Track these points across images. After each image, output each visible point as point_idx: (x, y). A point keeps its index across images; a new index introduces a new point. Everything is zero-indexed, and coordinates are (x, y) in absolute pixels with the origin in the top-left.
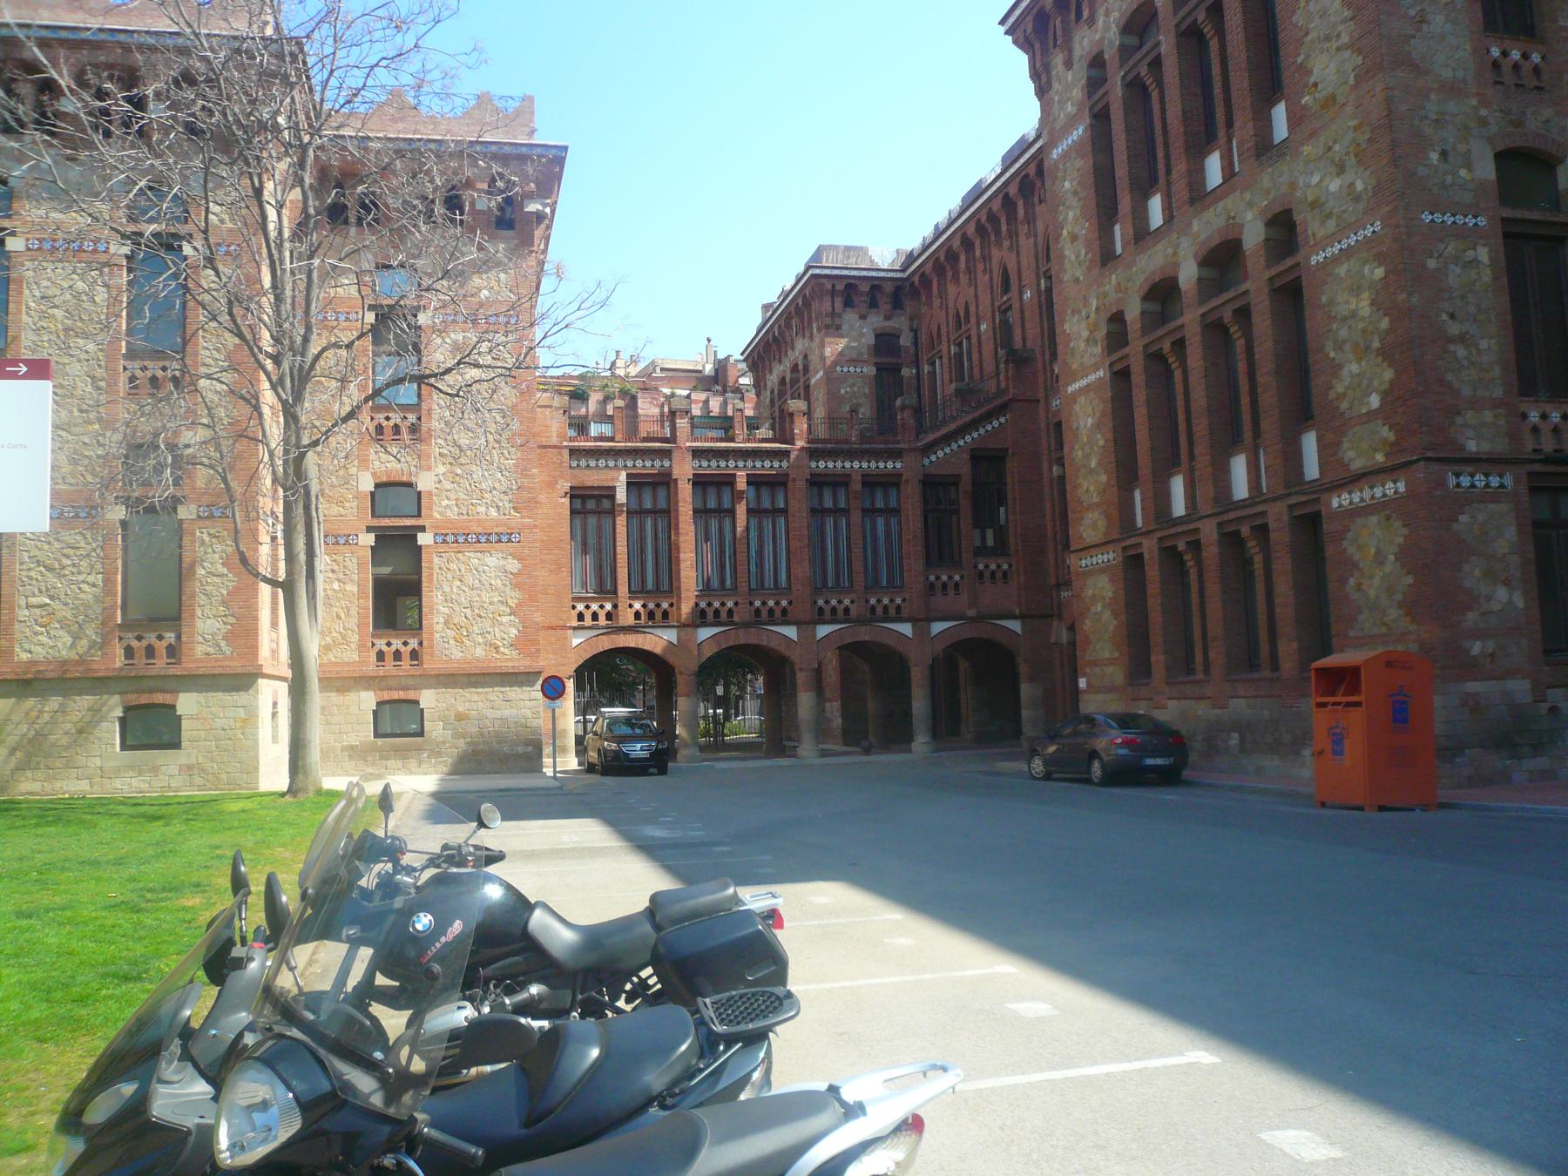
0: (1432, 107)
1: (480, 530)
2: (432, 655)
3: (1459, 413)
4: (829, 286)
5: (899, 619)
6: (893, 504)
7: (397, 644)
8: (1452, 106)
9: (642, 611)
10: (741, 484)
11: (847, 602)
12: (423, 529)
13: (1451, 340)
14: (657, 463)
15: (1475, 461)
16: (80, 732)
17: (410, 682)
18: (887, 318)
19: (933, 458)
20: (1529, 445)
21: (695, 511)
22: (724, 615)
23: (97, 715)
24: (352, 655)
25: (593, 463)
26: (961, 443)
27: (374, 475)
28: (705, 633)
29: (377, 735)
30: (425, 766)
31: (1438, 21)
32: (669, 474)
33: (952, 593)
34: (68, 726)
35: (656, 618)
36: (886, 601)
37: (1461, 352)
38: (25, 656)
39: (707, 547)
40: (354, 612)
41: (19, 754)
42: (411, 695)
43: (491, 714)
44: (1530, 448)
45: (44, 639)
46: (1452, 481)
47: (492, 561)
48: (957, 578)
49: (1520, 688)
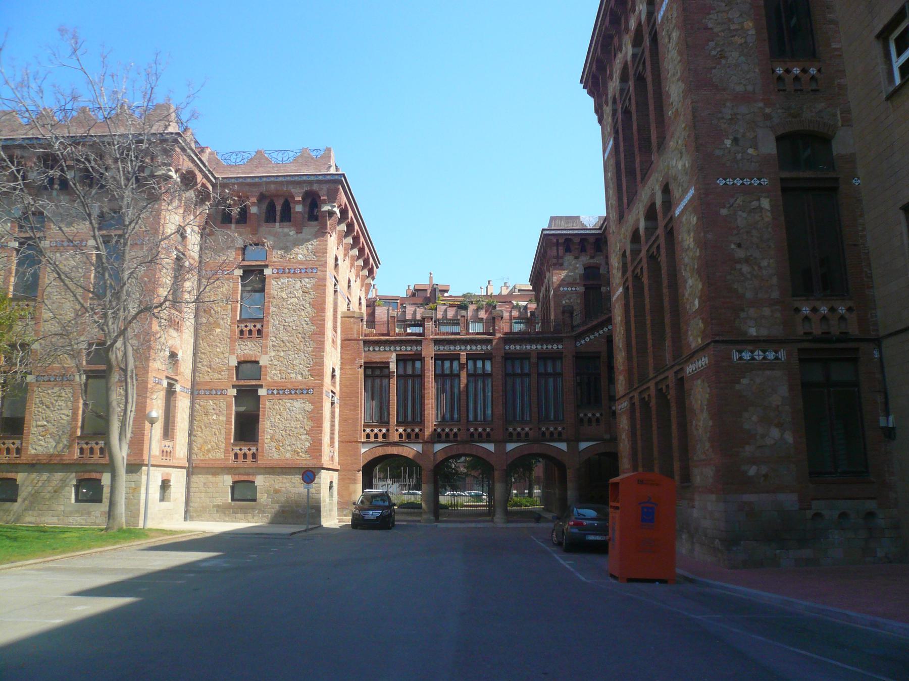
0: (727, 112)
1: (291, 387)
2: (263, 456)
3: (743, 310)
4: (555, 241)
5: (560, 440)
6: (559, 370)
7: (245, 450)
8: (743, 109)
9: (403, 433)
10: (463, 360)
11: (527, 429)
12: (261, 386)
13: (739, 261)
14: (414, 348)
15: (755, 342)
16: (55, 492)
17: (251, 471)
18: (592, 257)
19: (583, 342)
20: (800, 330)
21: (436, 375)
22: (451, 436)
23: (64, 484)
24: (220, 455)
25: (377, 349)
26: (601, 332)
27: (237, 357)
28: (438, 447)
29: (233, 499)
30: (256, 518)
31: (734, 56)
32: (421, 354)
33: (594, 424)
34: (50, 489)
35: (411, 437)
36: (552, 429)
37: (745, 269)
38: (33, 452)
39: (444, 396)
40: (223, 432)
41: (27, 502)
42: (251, 478)
43: (293, 490)
44: (802, 333)
45: (42, 443)
46: (735, 356)
47: (297, 404)
48: (598, 415)
49: (789, 500)
